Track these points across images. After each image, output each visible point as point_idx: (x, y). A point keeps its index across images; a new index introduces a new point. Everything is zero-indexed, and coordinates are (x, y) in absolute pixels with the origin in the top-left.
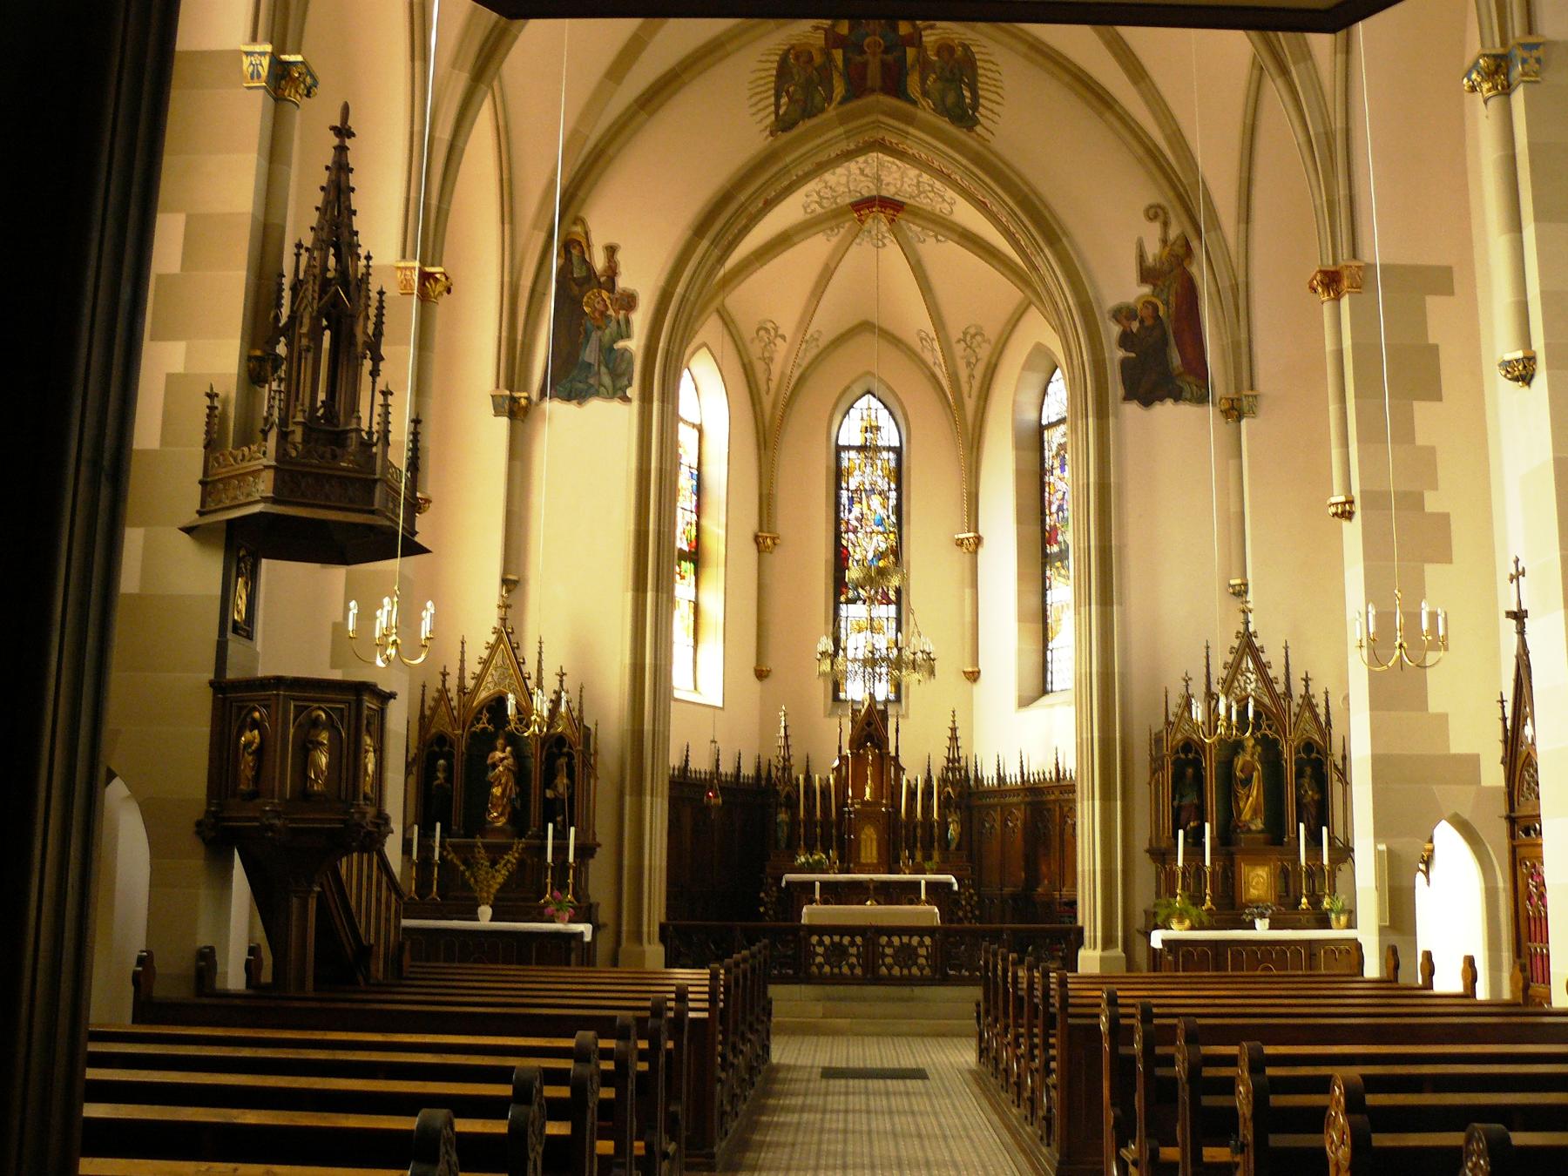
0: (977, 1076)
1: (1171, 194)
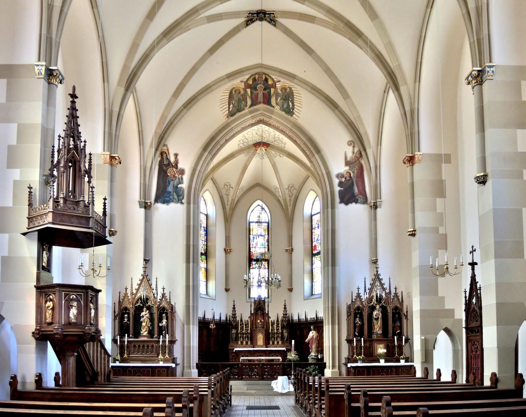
0: (295, 407)
1: (356, 137)
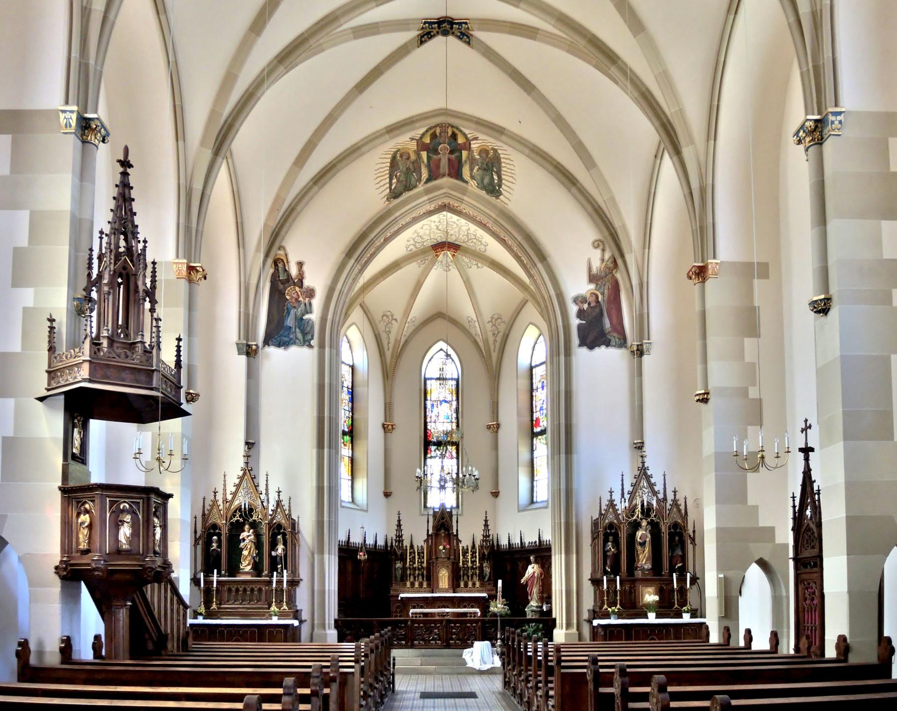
0: (503, 694)
1: (607, 234)
